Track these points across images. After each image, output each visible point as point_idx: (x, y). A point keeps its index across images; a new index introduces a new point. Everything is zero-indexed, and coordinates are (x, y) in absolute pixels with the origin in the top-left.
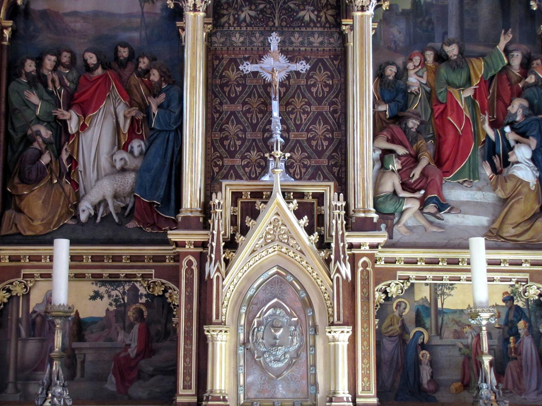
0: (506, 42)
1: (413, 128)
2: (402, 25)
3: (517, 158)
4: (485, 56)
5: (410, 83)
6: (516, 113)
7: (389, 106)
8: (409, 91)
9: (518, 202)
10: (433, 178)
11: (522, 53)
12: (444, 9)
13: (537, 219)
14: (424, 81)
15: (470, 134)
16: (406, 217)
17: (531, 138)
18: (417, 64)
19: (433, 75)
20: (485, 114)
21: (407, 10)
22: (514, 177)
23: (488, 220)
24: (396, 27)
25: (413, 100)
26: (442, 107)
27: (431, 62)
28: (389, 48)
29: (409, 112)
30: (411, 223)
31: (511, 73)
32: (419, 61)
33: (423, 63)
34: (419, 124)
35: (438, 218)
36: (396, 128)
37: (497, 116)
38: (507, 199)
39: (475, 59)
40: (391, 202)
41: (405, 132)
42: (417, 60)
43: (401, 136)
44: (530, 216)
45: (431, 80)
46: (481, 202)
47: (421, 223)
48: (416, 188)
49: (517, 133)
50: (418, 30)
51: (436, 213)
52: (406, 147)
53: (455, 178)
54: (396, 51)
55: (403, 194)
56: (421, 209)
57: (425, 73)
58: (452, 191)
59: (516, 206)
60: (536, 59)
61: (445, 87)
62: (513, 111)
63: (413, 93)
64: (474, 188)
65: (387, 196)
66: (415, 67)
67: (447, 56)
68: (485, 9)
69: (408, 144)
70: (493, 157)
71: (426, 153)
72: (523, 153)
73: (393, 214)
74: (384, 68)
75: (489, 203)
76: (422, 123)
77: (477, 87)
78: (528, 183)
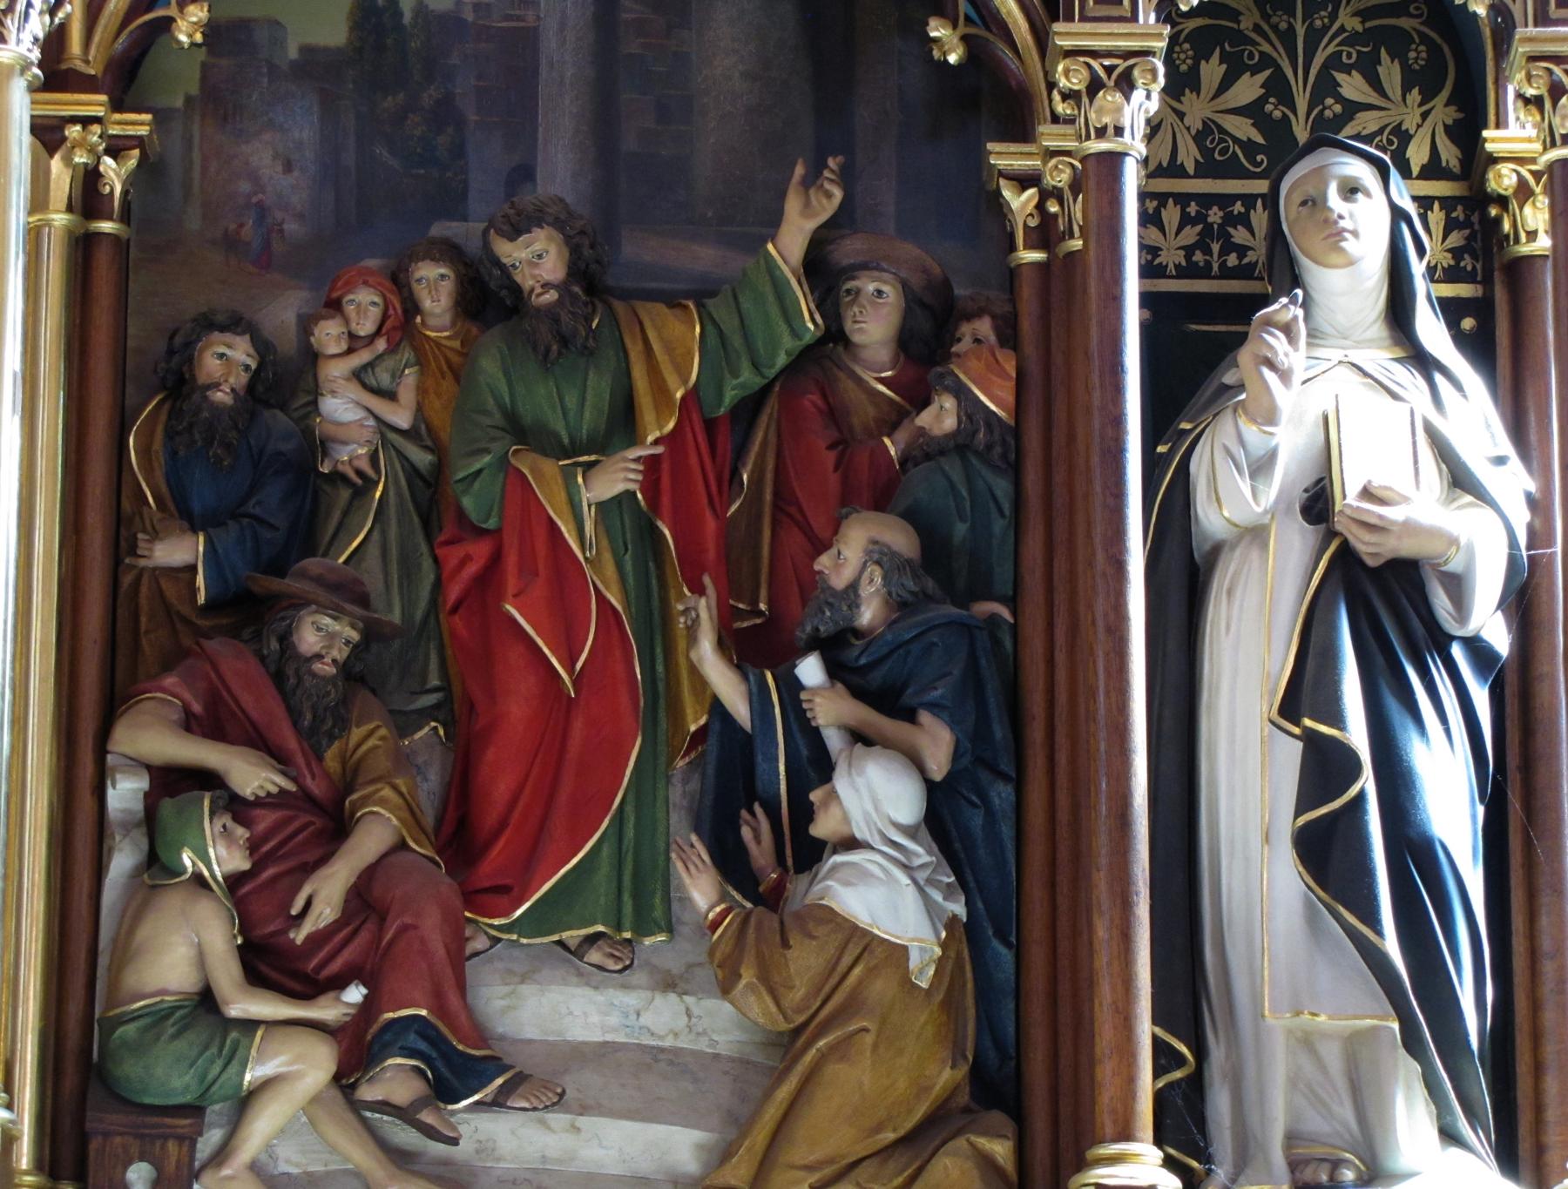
0: (811, 225)
1: (319, 657)
2: (301, 126)
3: (846, 819)
4: (713, 294)
5: (331, 430)
6: (853, 587)
7: (209, 543)
8: (325, 469)
9: (840, 1050)
10: (408, 920)
11: (905, 286)
12: (518, 52)
13: (944, 1143)
14: (401, 418)
15: (624, 699)
16: (262, 1126)
17: (925, 717)
18: (366, 328)
19: (448, 385)
20: (699, 590)
21: (326, 50)
22: (831, 917)
23: (700, 1147)
24: (267, 137)
25: (346, 513)
26: (480, 551)
27: (447, 319)
28: (231, 243)
29: (304, 575)
30: (291, 1160)
31: (848, 385)
32: (375, 313)
33: (403, 320)
34: (355, 636)
35: (430, 1132)
36: (235, 664)
37: (770, 603)
38: (797, 1031)
39: (661, 308)
40: (181, 1045)
41: (278, 678)
42: (366, 306)
43: (256, 698)
44: (910, 1124)
45: (440, 416)
46: (676, 1051)
47: (347, 1159)
48: (326, 972)
49: (859, 694)
50: (381, 151)
51: (419, 1104)
52: (279, 757)
53: (537, 922)
54: (265, 260)
55: (245, 1004)
56: (345, 1079)
57: (411, 375)
58: (525, 989)
59: (833, 1070)
60: (969, 317)
61: (497, 447)
62: (839, 581)
63: (344, 478)
64: (638, 976)
65: (159, 1017)
66: (354, 343)
67: (516, 290)
68: (731, 49)
69: (291, 742)
70: (744, 813)
71: (387, 792)
72: (876, 796)
73: (195, 1111)
74: (189, 345)
75: (716, 1056)
76: (372, 634)
77: (660, 450)
78: (899, 953)
